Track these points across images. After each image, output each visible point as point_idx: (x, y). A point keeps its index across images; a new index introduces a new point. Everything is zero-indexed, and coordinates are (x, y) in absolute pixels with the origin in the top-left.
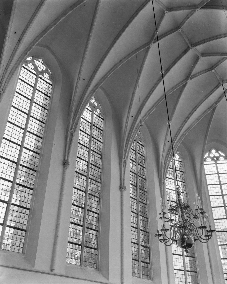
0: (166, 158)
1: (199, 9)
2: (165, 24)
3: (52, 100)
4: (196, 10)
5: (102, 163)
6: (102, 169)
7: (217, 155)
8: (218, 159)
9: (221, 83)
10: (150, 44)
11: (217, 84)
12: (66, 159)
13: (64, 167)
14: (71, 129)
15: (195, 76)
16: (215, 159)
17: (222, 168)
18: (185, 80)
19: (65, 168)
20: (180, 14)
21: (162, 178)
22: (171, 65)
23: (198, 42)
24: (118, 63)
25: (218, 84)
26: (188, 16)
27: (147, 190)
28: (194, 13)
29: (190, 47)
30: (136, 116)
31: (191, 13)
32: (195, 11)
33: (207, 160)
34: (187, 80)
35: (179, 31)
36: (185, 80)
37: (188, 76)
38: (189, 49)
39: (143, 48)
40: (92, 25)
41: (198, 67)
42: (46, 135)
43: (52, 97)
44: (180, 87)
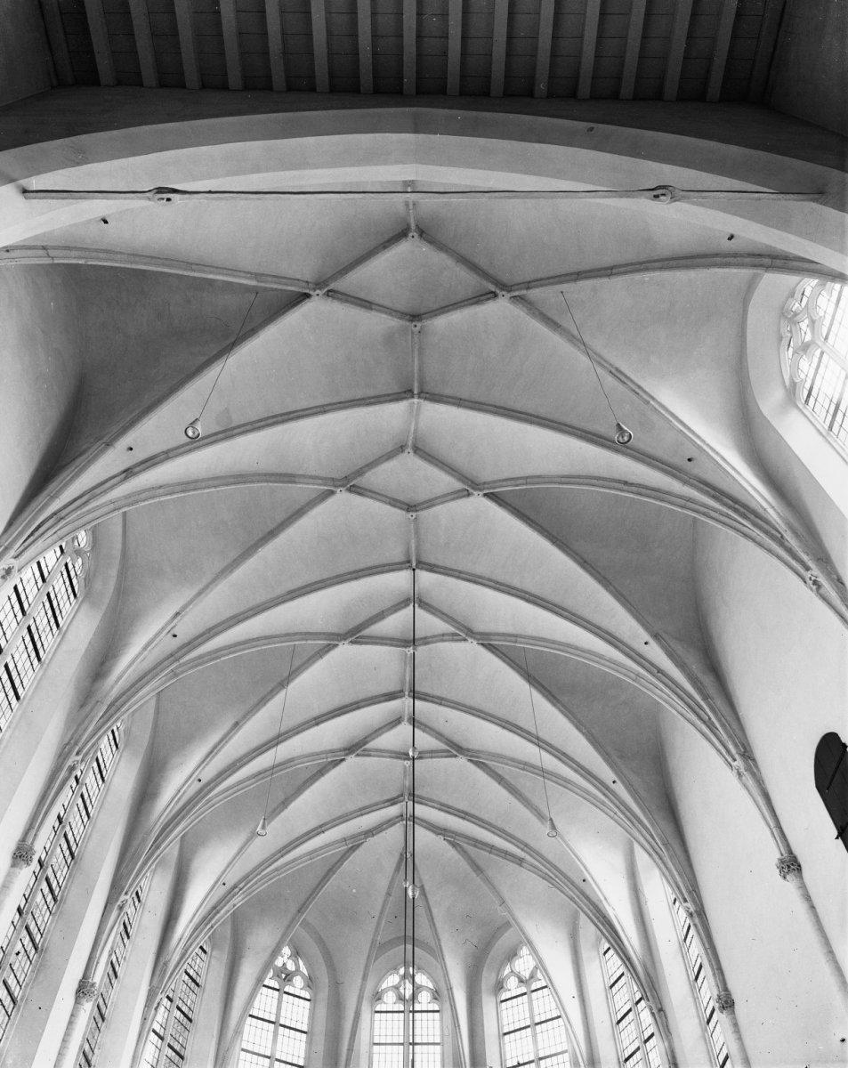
0: (196, 929)
1: (475, 642)
2: (394, 624)
3: (62, 639)
4: (470, 640)
5: (67, 884)
6: (60, 903)
7: (291, 966)
8: (289, 977)
9: (406, 797)
10: (341, 640)
11: (395, 794)
12: (29, 841)
13: (13, 865)
14: (78, 754)
15: (367, 754)
16: (283, 976)
17: (561, 1066)
18: (347, 752)
19: (17, 870)
20: (437, 625)
21: (160, 989)
22: (346, 706)
23: (427, 695)
24: (258, 639)
25: (398, 797)
26: (442, 637)
27: (109, 1012)
28: (460, 640)
29: (407, 693)
30: (208, 784)
31: (454, 637)
32: (465, 640)
33: (385, 999)
34: (347, 755)
35: (407, 650)
36: (345, 749)
37: (356, 747)
38: (401, 697)
39: (325, 639)
40: (272, 534)
41: (388, 740)
42: (10, 737)
43: (66, 631)
44: (333, 759)
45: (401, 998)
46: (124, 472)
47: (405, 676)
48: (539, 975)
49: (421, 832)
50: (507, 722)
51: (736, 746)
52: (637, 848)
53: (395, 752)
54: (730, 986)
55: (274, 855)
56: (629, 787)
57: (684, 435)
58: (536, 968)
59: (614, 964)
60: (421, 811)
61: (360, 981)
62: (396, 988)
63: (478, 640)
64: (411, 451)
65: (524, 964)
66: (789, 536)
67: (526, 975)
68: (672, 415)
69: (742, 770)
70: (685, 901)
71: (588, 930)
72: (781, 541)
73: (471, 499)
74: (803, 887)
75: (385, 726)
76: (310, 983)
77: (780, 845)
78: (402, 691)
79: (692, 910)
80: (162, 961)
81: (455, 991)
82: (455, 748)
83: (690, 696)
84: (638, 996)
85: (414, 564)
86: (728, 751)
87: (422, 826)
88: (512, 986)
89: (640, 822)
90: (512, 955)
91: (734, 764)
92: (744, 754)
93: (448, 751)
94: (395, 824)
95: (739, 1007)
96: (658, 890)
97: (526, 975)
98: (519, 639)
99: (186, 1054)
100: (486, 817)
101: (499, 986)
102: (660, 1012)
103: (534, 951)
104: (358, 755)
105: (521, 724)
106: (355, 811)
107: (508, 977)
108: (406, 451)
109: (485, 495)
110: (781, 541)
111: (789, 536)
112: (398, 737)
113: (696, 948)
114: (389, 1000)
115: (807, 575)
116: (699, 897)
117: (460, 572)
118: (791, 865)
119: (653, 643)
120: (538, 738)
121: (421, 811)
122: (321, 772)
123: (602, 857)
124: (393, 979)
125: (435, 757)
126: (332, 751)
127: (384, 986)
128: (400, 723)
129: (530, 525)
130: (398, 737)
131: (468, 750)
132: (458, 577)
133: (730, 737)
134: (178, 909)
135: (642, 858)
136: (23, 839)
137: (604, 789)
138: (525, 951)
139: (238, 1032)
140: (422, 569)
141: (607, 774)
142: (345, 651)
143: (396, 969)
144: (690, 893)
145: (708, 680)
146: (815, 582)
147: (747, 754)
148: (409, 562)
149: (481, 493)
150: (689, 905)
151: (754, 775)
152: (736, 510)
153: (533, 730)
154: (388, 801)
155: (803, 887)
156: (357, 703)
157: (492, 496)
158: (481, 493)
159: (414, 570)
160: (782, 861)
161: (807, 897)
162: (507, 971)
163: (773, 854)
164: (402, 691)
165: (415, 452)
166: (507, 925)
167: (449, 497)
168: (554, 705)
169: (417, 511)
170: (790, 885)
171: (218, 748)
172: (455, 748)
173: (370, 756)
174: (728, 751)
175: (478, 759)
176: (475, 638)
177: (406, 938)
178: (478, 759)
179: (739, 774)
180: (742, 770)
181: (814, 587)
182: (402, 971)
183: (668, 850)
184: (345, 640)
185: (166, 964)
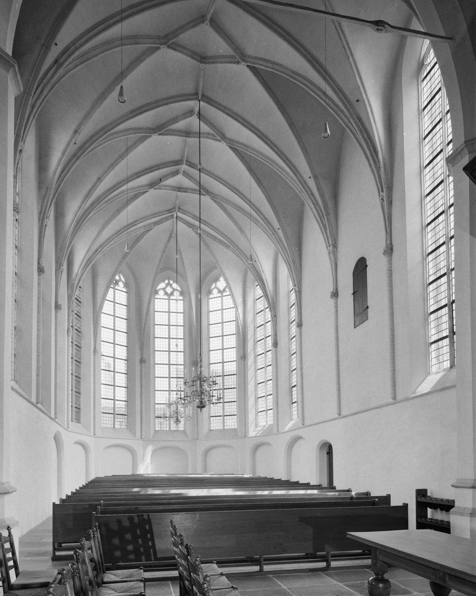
1: (225, 144)
4: (223, 142)
18: (149, 187)
25: (172, 209)
34: (149, 188)
36: (148, 185)
45: (166, 293)
46: (200, 299)
47: (184, 152)
48: (227, 290)
49: (181, 225)
50: (234, 188)
51: (332, 241)
52: (280, 259)
53: (174, 187)
55: (113, 235)
56: (285, 233)
57: (358, 89)
58: (226, 287)
59: (259, 292)
61: (150, 288)
62: (164, 289)
63: (227, 143)
64: (209, 23)
65: (221, 284)
66: (382, 169)
67: (222, 289)
68: (358, 70)
69: (331, 252)
70: (295, 286)
71: (251, 277)
72: (378, 169)
73: (239, 66)
74: (336, 304)
75: (170, 174)
76: (126, 285)
78: (182, 160)
79: (297, 290)
80: (70, 283)
81: (192, 295)
83: (321, 211)
84: (267, 306)
85: (200, 97)
86: (328, 242)
87: (182, 222)
88: (215, 291)
89: (282, 242)
90: (216, 280)
91: (329, 248)
92: (334, 244)
94: (169, 220)
95: (303, 327)
96: (284, 271)
97: (222, 289)
98: (249, 150)
99: (81, 315)
100: (215, 225)
102: (275, 317)
103: (226, 280)
104: (155, 189)
105: (241, 189)
106: (151, 215)
107: (214, 288)
108: (206, 23)
109: (248, 66)
110: (378, 171)
111: (382, 169)
112: (179, 180)
113: (293, 297)
114: (161, 293)
115: (381, 194)
116: (301, 285)
117: (225, 108)
118: (335, 294)
119: (312, 179)
120: (250, 202)
122: (136, 197)
123: (265, 254)
124: (162, 285)
125: (194, 193)
126: (142, 186)
127: (159, 287)
129: (269, 94)
131: (211, 193)
132: (223, 111)
133: (331, 236)
134: (72, 258)
135: (280, 259)
137: (273, 231)
138: (222, 279)
139: (101, 307)
140: (204, 101)
141: (276, 225)
142: (155, 139)
143: (163, 281)
144: (298, 283)
145: (330, 204)
146: (382, 199)
147: (335, 246)
148: (197, 94)
149: (246, 64)
150: (296, 288)
151: (334, 255)
152: (367, 144)
153: (249, 198)
154: (168, 211)
155: (336, 304)
156: (158, 165)
157: (254, 70)
158: (246, 64)
159: (199, 101)
160: (333, 292)
161: (336, 307)
162: (213, 286)
163: (331, 289)
164: (182, 160)
165: (211, 25)
166: (215, 267)
167: (226, 60)
168: (259, 186)
169: (205, 63)
170: (332, 301)
171: (92, 192)
173: (160, 189)
174: (328, 242)
176: (225, 142)
177: (170, 268)
179: (329, 253)
180: (331, 252)
181: (381, 201)
182: (167, 282)
183: (294, 264)
185: (72, 285)
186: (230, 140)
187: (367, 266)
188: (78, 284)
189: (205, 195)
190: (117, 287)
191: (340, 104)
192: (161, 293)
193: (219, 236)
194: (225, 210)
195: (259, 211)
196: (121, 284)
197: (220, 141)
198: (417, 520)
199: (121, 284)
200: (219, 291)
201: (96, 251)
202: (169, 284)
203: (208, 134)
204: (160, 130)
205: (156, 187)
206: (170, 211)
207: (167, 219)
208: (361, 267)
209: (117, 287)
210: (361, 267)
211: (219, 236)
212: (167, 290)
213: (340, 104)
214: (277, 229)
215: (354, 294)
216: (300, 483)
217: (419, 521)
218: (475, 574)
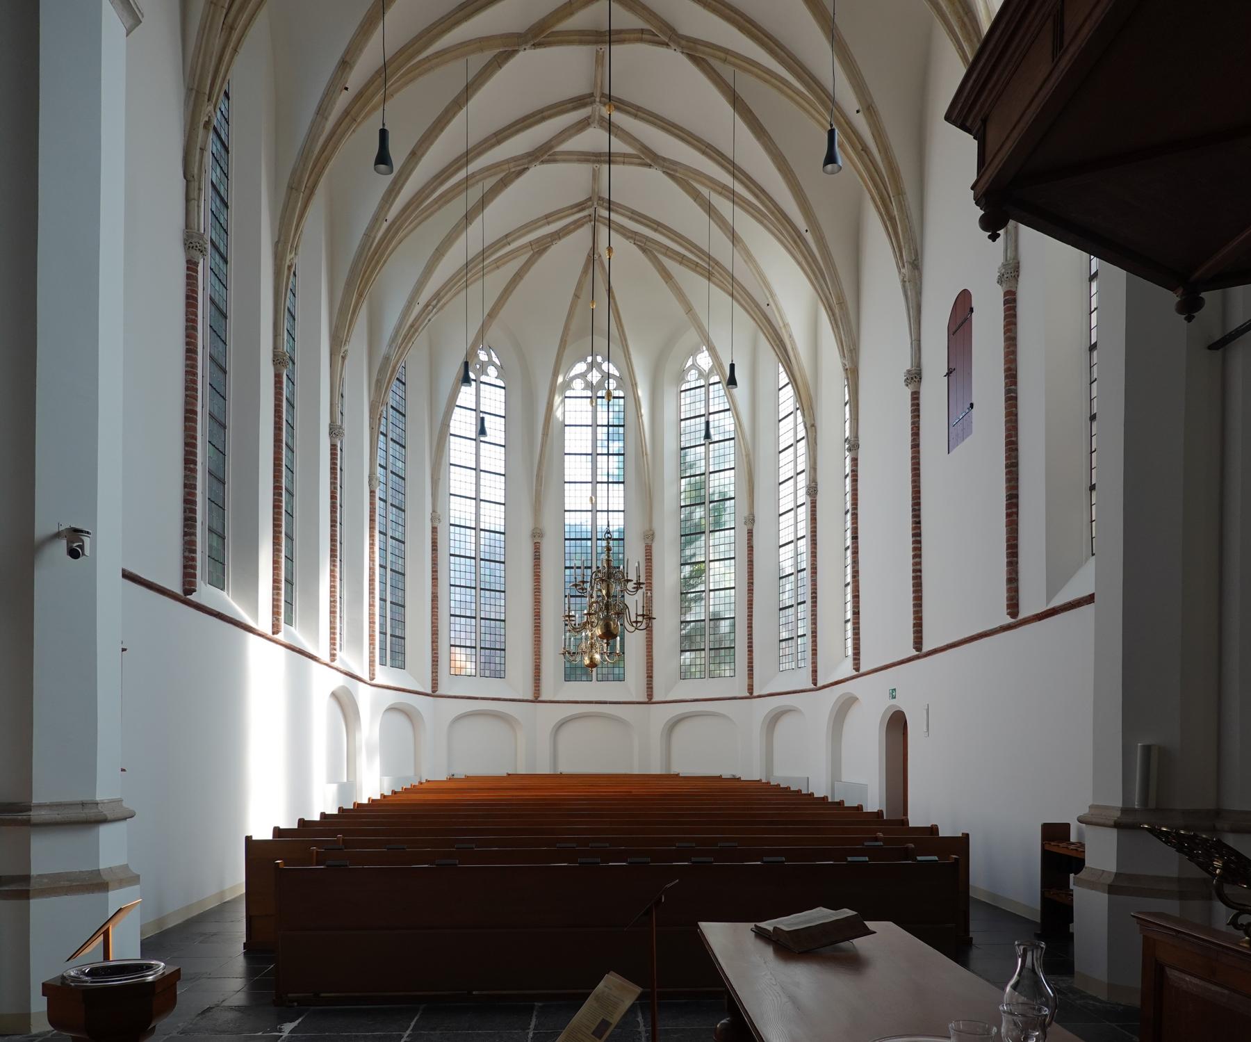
34: (530, 162)
45: (589, 386)
54: (819, 480)
60: (637, 186)
62: (583, 376)
76: (502, 372)
77: (1085, 30)
82: (648, 157)
93: (640, 158)
101: (681, 376)
104: (543, 162)
112: (593, 138)
114: (578, 384)
121: (637, 186)
124: (580, 367)
128: (589, 124)
130: (593, 138)
131: (664, 159)
136: (187, 225)
142: (527, 58)
162: (690, 363)
164: (592, 95)
172: (648, 157)
174: (901, 255)
175: (672, 170)
178: (672, 170)
182: (589, 359)
184: (526, 43)
186: (688, 39)
187: (972, 310)
188: (393, 371)
189: (650, 166)
190: (483, 378)
191: (803, 89)
192: (578, 384)
193: (739, 188)
194: (696, 196)
195: (763, 191)
196: (492, 371)
197: (667, 45)
198: (1043, 846)
199: (492, 371)
200: (701, 374)
201: (427, 306)
202: (592, 366)
203: (642, 31)
204: (536, 36)
205: (546, 157)
206: (580, 206)
207: (577, 225)
208: (963, 308)
209: (483, 378)
210: (963, 308)
211: (739, 188)
212: (589, 377)
213: (803, 89)
214: (803, 232)
215: (948, 374)
216: (846, 805)
217: (1047, 847)
218: (1039, 920)
